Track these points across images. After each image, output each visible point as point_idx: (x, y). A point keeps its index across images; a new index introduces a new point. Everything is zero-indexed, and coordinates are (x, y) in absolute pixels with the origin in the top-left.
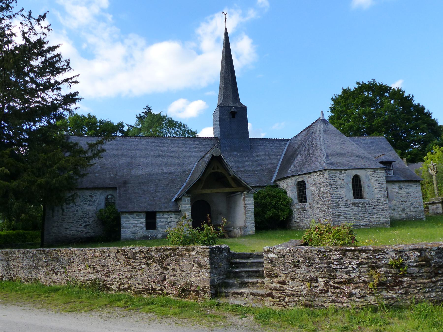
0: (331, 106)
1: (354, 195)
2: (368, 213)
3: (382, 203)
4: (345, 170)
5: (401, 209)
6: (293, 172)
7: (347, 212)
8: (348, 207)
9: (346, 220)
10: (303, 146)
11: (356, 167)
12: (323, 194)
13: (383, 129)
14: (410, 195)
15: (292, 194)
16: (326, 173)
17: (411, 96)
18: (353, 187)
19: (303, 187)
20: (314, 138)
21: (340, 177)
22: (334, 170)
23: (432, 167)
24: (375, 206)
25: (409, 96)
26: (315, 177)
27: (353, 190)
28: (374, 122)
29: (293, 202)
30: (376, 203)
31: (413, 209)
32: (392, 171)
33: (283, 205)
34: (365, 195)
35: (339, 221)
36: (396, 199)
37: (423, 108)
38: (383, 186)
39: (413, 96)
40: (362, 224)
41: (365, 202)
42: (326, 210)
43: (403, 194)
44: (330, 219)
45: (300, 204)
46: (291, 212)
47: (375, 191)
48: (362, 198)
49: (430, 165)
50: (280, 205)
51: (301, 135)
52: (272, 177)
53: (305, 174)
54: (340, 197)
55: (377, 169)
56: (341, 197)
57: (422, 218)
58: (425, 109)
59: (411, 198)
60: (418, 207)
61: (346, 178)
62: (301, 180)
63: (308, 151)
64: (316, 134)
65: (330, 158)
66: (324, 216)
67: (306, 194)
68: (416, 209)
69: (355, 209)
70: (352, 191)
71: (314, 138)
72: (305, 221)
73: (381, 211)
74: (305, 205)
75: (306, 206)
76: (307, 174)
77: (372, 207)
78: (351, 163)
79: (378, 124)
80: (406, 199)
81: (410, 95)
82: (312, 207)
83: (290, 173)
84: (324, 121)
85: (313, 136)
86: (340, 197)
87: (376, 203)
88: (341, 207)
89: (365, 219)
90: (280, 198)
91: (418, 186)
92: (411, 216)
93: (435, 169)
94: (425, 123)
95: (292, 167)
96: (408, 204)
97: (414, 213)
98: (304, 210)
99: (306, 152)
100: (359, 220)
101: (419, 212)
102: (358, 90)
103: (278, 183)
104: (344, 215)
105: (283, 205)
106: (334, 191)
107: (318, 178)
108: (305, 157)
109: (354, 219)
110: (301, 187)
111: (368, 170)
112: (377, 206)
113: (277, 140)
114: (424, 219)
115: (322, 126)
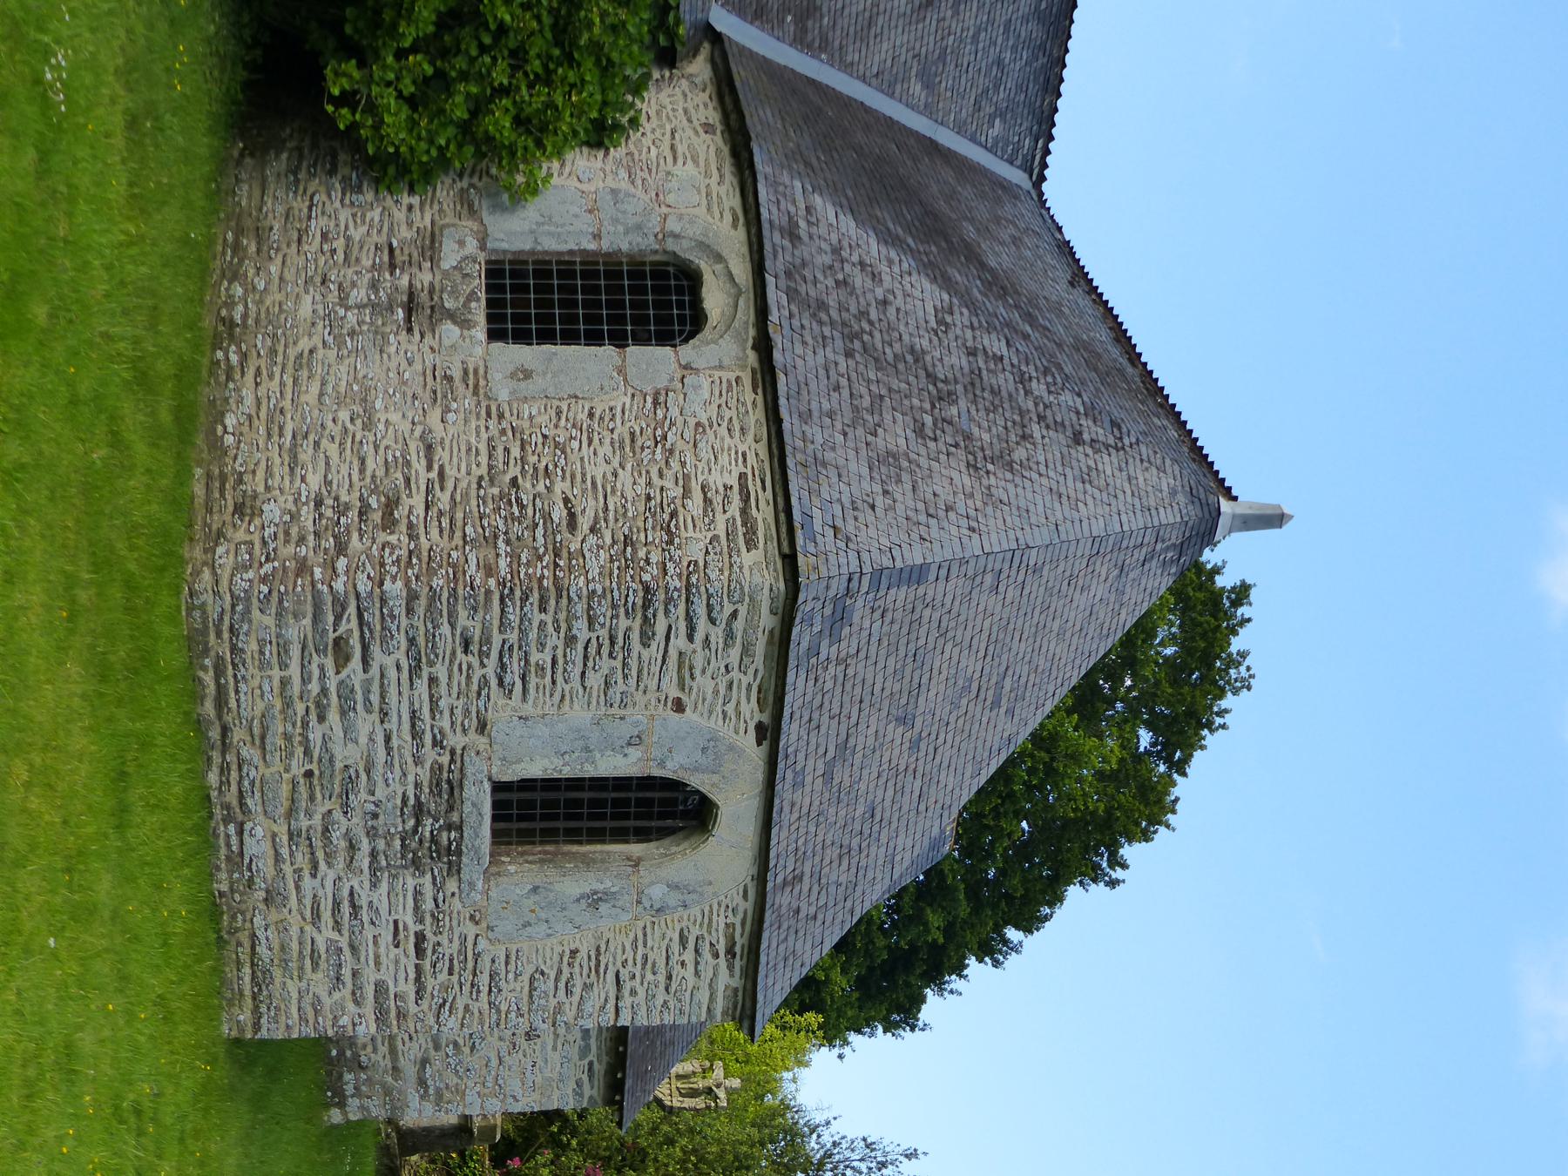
1: (527, 784)
2: (360, 883)
4: (770, 733)
6: (792, 234)
7: (365, 724)
8: (416, 734)
9: (288, 704)
10: (1010, 332)
11: (785, 818)
12: (559, 513)
15: (579, 203)
16: (757, 570)
17: (1118, 873)
18: (599, 783)
19: (640, 320)
20: (1077, 439)
21: (703, 683)
22: (781, 642)
23: (701, 1084)
24: (420, 938)
26: (729, 456)
27: (576, 784)
29: (498, 207)
30: (450, 948)
33: (478, 108)
35: (283, 649)
37: (1030, 923)
38: (592, 1004)
39: (1113, 884)
41: (454, 869)
42: (399, 537)
44: (303, 568)
45: (478, 272)
46: (404, 171)
49: (719, 1072)
50: (481, 78)
51: (1079, 296)
52: (758, 15)
53: (764, 346)
54: (515, 667)
56: (514, 676)
57: (342, 1105)
60: (422, 1082)
61: (696, 731)
62: (714, 299)
63: (974, 382)
64: (1108, 463)
65: (900, 595)
66: (342, 509)
67: (570, 338)
69: (393, 787)
70: (567, 772)
71: (1077, 439)
72: (305, 309)
73: (370, 976)
74: (465, 324)
75: (450, 331)
76: (766, 375)
77: (408, 918)
78: (828, 776)
81: (1124, 866)
82: (441, 387)
83: (788, 193)
84: (1206, 533)
85: (1090, 430)
86: (515, 667)
87: (450, 948)
88: (415, 671)
89: (302, 860)
90: (547, 79)
91: (578, 1093)
93: (689, 1103)
95: (833, 222)
97: (381, 1058)
98: (418, 311)
99: (958, 360)
100: (291, 813)
101: (387, 1092)
102: (1200, 587)
103: (699, 67)
104: (346, 692)
105: (478, 108)
106: (581, 629)
107: (717, 480)
108: (918, 356)
109: (297, 769)
110: (638, 300)
112: (420, 952)
113: (1052, 84)
114: (336, 1116)
115: (1168, 517)
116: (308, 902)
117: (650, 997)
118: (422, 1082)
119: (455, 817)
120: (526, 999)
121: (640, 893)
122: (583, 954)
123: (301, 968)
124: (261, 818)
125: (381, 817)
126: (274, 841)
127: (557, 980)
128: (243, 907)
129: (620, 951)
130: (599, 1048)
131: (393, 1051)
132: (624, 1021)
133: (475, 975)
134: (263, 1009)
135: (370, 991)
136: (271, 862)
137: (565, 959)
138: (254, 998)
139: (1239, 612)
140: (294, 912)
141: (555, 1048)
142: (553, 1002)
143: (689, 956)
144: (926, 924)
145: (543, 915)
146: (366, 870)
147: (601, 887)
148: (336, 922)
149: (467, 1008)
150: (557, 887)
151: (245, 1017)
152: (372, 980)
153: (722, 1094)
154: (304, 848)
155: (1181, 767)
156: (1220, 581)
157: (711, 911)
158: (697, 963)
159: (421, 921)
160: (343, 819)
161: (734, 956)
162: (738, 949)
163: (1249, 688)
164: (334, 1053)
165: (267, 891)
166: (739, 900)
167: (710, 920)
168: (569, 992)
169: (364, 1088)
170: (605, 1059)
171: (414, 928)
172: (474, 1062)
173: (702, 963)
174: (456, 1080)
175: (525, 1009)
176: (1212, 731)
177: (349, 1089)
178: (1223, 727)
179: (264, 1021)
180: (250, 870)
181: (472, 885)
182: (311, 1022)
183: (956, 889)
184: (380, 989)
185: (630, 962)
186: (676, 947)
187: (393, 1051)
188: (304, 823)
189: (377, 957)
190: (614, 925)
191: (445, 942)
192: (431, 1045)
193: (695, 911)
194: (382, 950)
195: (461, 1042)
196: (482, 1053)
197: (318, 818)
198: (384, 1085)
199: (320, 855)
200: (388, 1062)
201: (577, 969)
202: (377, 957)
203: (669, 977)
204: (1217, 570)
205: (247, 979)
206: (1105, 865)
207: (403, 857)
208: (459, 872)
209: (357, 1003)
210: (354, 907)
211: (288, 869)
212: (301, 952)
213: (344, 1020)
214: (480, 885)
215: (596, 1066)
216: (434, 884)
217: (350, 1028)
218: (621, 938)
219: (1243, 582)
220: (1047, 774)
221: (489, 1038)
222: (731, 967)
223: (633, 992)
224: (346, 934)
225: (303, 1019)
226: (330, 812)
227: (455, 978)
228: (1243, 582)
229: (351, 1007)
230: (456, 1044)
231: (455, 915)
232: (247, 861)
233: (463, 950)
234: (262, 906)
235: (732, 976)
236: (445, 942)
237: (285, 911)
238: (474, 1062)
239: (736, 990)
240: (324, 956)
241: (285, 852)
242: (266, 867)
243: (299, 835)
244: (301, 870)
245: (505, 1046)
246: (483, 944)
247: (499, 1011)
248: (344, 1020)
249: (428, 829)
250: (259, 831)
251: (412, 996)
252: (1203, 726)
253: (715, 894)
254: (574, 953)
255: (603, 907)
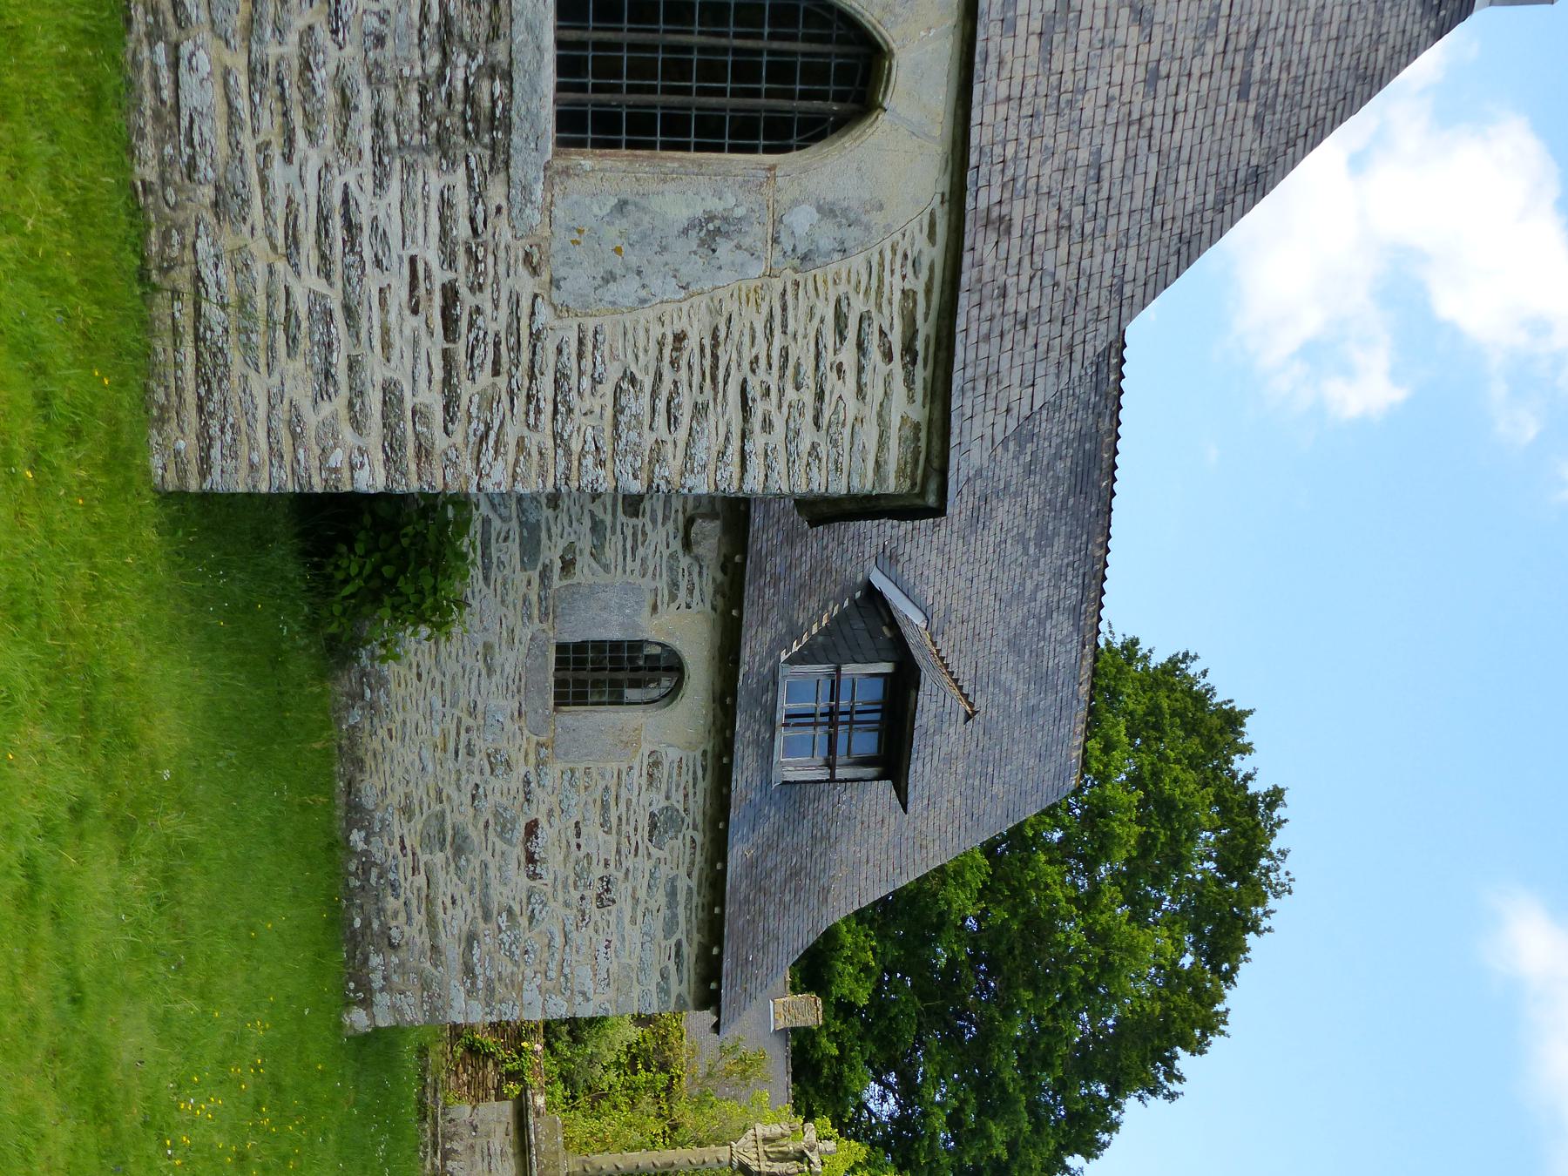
0: (1143, 648)
2: (355, 176)
3: (489, 401)
5: (460, 814)
13: (999, 914)
14: (591, 907)
17: (1175, 1087)
23: (791, 1147)
24: (450, 294)
25: (1172, 1075)
28: (1050, 862)
30: (495, 322)
31: (455, 922)
32: (823, 774)
34: (606, 174)
36: (554, 770)
39: (1172, 1096)
40: (204, 55)
41: (500, 159)
43: (598, 841)
47: (651, 327)
48: (574, 127)
55: (940, 393)
57: (367, 1003)
58: (1089, 1155)
59: (555, 915)
60: (469, 970)
68: (453, 951)
73: (376, 371)
79: (1035, 883)
80: (554, 863)
81: (1180, 1079)
87: (495, 322)
89: (270, 127)
91: (664, 991)
92: (391, 903)
94: (1011, 1146)
96: (511, 885)
111: (934, 254)
114: (358, 1019)
116: (279, 211)
117: (793, 435)
118: (469, 970)
119: (500, 52)
120: (608, 430)
121: (778, 221)
122: (692, 343)
123: (271, 348)
124: (205, 35)
125: (389, 43)
126: (226, 84)
127: (654, 395)
128: (180, 216)
129: (747, 340)
130: (689, 921)
131: (431, 921)
132: (754, 484)
133: (532, 377)
134: (215, 430)
135: (375, 399)
136: (221, 127)
137: (667, 351)
138: (200, 409)
139: (1275, 815)
140: (259, 232)
141: (633, 921)
142: (649, 439)
143: (848, 355)
144: (989, 1138)
145: (633, 260)
146: (367, 154)
147: (715, 205)
148: (323, 257)
149: (520, 443)
150: (655, 203)
151: (187, 444)
152: (378, 379)
153: (815, 1159)
154: (271, 101)
155: (1228, 977)
156: (1253, 788)
157: (882, 265)
158: (860, 369)
159: (452, 265)
160: (331, 47)
161: (914, 362)
162: (920, 345)
163: (1290, 892)
164: (357, 923)
165: (217, 188)
166: (922, 241)
167: (881, 281)
168: (673, 421)
169: (395, 978)
170: (696, 937)
171: (440, 276)
172: (532, 938)
173: (869, 369)
174: (510, 968)
175: (607, 449)
176: (1258, 933)
177: (377, 980)
178: (1269, 930)
179: (215, 453)
180: (191, 143)
181: (526, 189)
182: (287, 458)
183: (1017, 1101)
184: (391, 394)
185: (763, 362)
186: (829, 338)
187: (431, 921)
188: (273, 51)
189: (386, 331)
190: (736, 275)
191: (488, 307)
192: (479, 913)
193: (857, 262)
194: (393, 317)
195: (517, 909)
196: (543, 927)
197: (293, 38)
198: (420, 973)
199: (297, 117)
200: (425, 937)
201: (683, 374)
202: (386, 331)
203: (820, 396)
204: (1248, 777)
205: (189, 369)
206: (1162, 1078)
207: (423, 128)
208: (507, 164)
209: (357, 425)
210: (350, 226)
211: (248, 143)
212: (270, 314)
213: (337, 458)
214: (538, 189)
215: (685, 949)
216: (470, 187)
217: (346, 474)
218: (749, 311)
219: (1275, 787)
220: (1103, 971)
221: (552, 904)
222: (909, 382)
223: (767, 425)
224: (339, 284)
225: (275, 453)
226: (311, 28)
227: (502, 381)
228: (1275, 787)
229: (347, 432)
230: (510, 911)
231: (502, 254)
232: (185, 123)
233: (513, 328)
234: (209, 217)
235: (911, 400)
236: (488, 307)
237: (246, 229)
238: (532, 938)
239: (917, 427)
240: (304, 324)
241: (242, 104)
242: (213, 131)
243: (265, 73)
244: (268, 144)
245: (572, 914)
246: (544, 315)
247: (568, 453)
248: (337, 458)
249: (460, 74)
250: (202, 59)
251: (438, 415)
252: (1247, 930)
253: (887, 227)
254: (680, 338)
255: (724, 248)
